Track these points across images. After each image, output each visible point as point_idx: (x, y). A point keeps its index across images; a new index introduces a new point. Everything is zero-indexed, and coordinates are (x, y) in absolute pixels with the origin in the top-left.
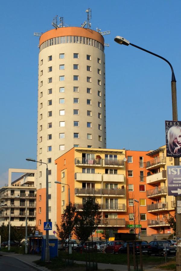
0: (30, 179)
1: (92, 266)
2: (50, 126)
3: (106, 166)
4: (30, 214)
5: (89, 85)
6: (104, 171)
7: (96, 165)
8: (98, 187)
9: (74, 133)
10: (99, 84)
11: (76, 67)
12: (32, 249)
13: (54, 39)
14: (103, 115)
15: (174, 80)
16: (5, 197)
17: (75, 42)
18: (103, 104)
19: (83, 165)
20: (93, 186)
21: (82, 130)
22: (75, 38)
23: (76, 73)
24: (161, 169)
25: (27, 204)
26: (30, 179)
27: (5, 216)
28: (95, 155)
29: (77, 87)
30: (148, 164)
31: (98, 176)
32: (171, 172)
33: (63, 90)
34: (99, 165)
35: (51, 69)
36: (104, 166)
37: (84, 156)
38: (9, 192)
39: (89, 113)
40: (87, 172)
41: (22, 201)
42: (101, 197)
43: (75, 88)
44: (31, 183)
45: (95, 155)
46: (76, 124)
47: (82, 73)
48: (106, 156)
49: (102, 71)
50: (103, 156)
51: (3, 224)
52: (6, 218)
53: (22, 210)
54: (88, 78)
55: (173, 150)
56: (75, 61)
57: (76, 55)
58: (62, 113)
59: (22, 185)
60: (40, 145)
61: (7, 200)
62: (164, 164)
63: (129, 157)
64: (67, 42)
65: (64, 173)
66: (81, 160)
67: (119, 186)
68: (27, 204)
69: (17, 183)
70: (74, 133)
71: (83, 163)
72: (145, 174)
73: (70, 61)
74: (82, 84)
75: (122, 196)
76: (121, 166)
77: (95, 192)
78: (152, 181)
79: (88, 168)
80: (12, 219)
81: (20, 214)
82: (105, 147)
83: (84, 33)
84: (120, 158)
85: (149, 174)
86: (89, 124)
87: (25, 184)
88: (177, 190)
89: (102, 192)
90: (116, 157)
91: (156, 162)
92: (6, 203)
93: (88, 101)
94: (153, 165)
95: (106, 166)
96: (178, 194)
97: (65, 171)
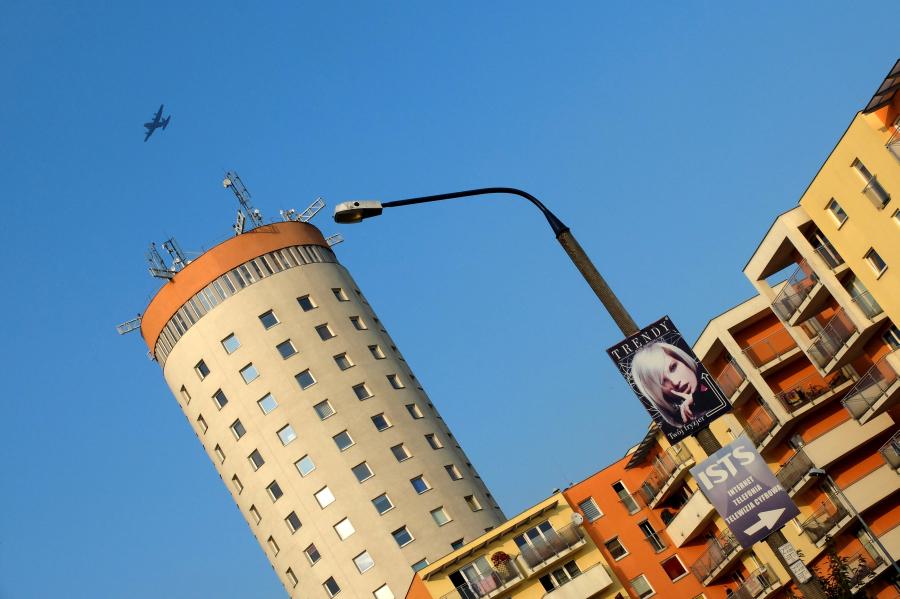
3: (537, 569)
5: (353, 377)
6: (539, 587)
13: (182, 312)
15: (560, 230)
17: (242, 284)
21: (409, 510)
22: (236, 274)
23: (296, 365)
29: (324, 402)
30: (646, 493)
32: (712, 479)
34: (516, 581)
35: (220, 397)
36: (530, 572)
37: (457, 580)
39: (398, 452)
43: (320, 408)
46: (381, 504)
47: (314, 354)
48: (520, 542)
50: (510, 548)
55: (676, 416)
56: (276, 335)
57: (268, 319)
58: (326, 497)
63: (582, 506)
72: (656, 523)
73: (260, 344)
74: (332, 384)
76: (579, 545)
78: (688, 533)
82: (502, 520)
83: (255, 246)
85: (668, 518)
86: (417, 483)
90: (546, 527)
93: (379, 422)
94: (661, 485)
95: (537, 569)
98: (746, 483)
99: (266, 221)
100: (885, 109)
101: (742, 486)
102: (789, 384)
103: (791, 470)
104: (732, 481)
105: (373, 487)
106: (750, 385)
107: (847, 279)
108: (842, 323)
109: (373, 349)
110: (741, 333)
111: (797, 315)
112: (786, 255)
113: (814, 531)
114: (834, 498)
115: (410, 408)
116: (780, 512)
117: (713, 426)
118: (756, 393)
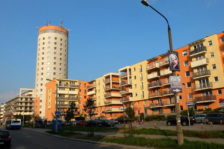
0: (30, 93)
1: (91, 134)
2: (43, 69)
3: (70, 87)
4: (30, 109)
5: (61, 52)
6: (69, 89)
7: (66, 87)
8: (66, 96)
9: (54, 73)
10: (65, 52)
11: (55, 43)
12: (37, 125)
13: (46, 30)
14: (67, 65)
15: (169, 29)
16: (18, 101)
17: (55, 32)
18: (67, 60)
19: (60, 86)
20: (64, 96)
21: (57, 71)
22: (56, 31)
23: (55, 46)
24: (94, 89)
25: (29, 105)
26: (30, 93)
27: (17, 110)
28: (65, 82)
29: (56, 52)
30: (88, 87)
31: (66, 91)
32: (172, 79)
33: (49, 53)
34: (67, 87)
35: (44, 43)
36: (69, 87)
37: (60, 82)
38: (20, 99)
39: (61, 64)
40: (61, 90)
41: (26, 103)
42: (67, 101)
43: (55, 53)
44: (31, 95)
45: (65, 82)
46: (55, 68)
47: (58, 46)
48: (70, 83)
49: (67, 46)
50: (69, 83)
51: (17, 114)
52: (18, 111)
53: (26, 107)
54: (61, 49)
55: (173, 67)
56: (55, 41)
57: (56, 38)
58: (49, 63)
59: (26, 96)
60: (37, 77)
61: (18, 103)
62: (96, 87)
63: (80, 83)
64: (52, 32)
65: (50, 90)
66: (59, 84)
67: (76, 96)
68: (29, 105)
69: (23, 95)
70: (54, 73)
71: (60, 86)
72: (87, 91)
73: (53, 41)
74: (58, 51)
75: (77, 100)
76: (77, 88)
77: (65, 99)
78: (90, 94)
79: (62, 88)
80: (21, 111)
81: (25, 109)
82: (67, 79)
83: (60, 29)
84: (76, 84)
85: (88, 91)
86: (60, 69)
87: (28, 95)
88: (176, 90)
89: (68, 99)
90: (74, 83)
91: (92, 86)
92: (18, 104)
93: (61, 59)
94: (90, 87)
95: (70, 87)
96: (177, 92)
97: (51, 89)
98: (177, 83)
99: (63, 27)
100: (149, 62)
101: (176, 83)
102: (114, 85)
103: (108, 95)
104: (175, 82)
105: (55, 66)
106: (110, 82)
107: (130, 77)
108: (223, 67)
109: (66, 50)
110: (113, 76)
111: (122, 78)
112: (125, 71)
113: (105, 103)
114: (110, 101)
115: (65, 60)
116: (179, 91)
117: (176, 72)
118: (110, 84)
